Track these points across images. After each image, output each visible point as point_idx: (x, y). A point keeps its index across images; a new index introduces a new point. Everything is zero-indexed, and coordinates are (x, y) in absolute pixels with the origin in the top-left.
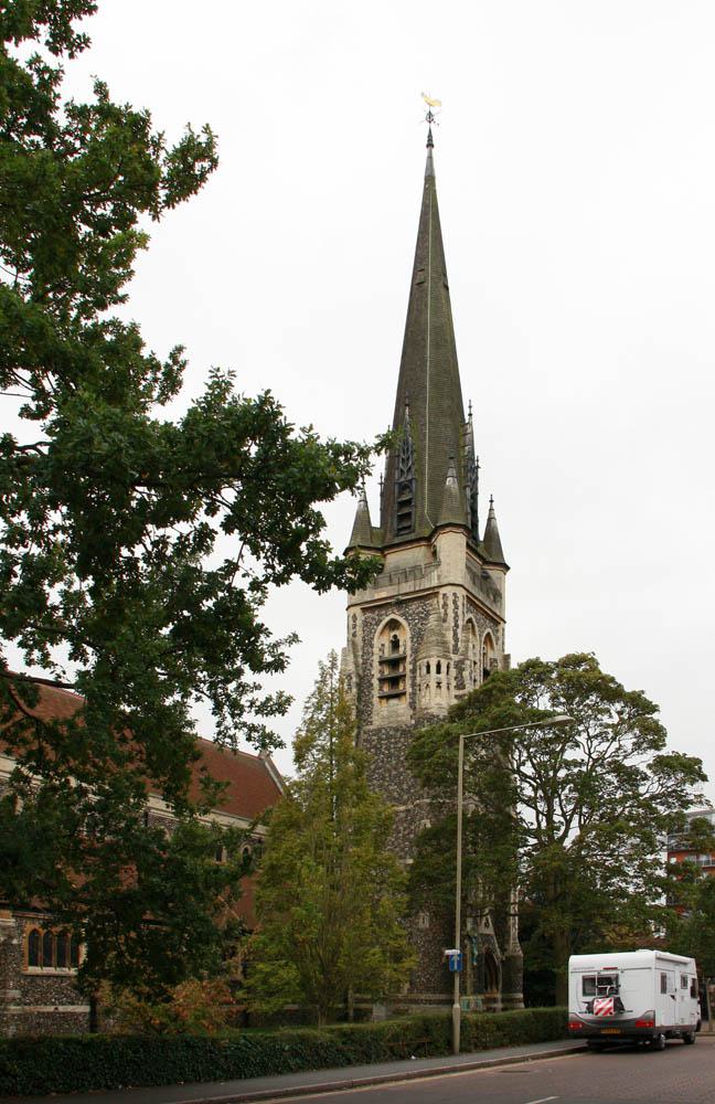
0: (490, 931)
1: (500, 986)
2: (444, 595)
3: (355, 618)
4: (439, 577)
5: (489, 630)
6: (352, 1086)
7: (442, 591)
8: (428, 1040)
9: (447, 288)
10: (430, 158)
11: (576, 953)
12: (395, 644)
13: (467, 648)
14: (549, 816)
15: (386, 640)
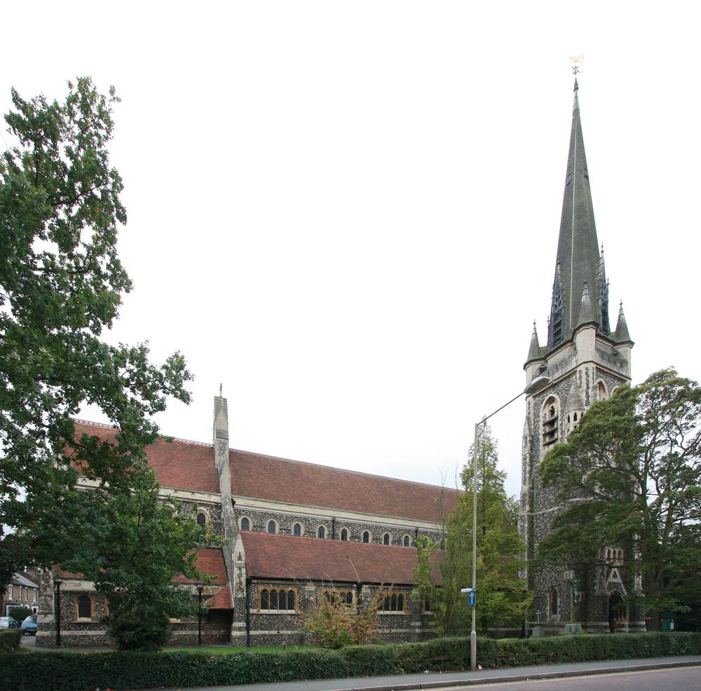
0: (618, 580)
3: (529, 403)
4: (576, 361)
7: (578, 369)
8: (445, 658)
9: (587, 177)
10: (576, 97)
12: (552, 412)
15: (547, 411)
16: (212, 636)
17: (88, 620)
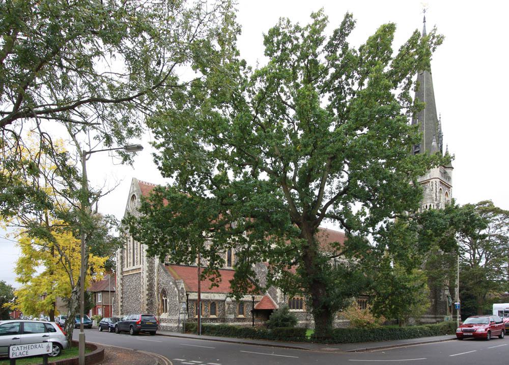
1: (452, 312)
2: (432, 182)
4: (430, 176)
5: (447, 191)
6: (441, 341)
7: (431, 181)
9: (431, 73)
11: (496, 303)
13: (440, 199)
14: (474, 255)
16: (259, 325)
17: (214, 316)
